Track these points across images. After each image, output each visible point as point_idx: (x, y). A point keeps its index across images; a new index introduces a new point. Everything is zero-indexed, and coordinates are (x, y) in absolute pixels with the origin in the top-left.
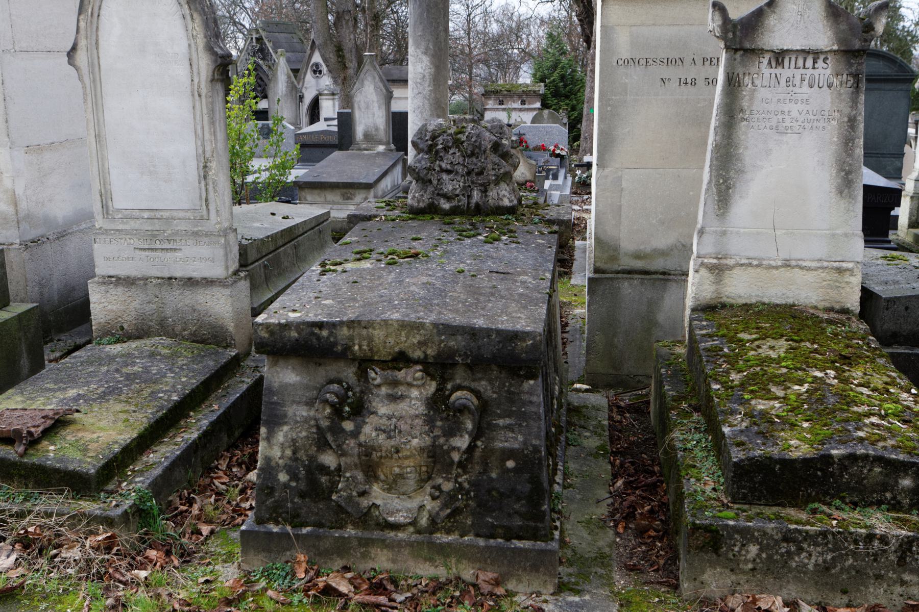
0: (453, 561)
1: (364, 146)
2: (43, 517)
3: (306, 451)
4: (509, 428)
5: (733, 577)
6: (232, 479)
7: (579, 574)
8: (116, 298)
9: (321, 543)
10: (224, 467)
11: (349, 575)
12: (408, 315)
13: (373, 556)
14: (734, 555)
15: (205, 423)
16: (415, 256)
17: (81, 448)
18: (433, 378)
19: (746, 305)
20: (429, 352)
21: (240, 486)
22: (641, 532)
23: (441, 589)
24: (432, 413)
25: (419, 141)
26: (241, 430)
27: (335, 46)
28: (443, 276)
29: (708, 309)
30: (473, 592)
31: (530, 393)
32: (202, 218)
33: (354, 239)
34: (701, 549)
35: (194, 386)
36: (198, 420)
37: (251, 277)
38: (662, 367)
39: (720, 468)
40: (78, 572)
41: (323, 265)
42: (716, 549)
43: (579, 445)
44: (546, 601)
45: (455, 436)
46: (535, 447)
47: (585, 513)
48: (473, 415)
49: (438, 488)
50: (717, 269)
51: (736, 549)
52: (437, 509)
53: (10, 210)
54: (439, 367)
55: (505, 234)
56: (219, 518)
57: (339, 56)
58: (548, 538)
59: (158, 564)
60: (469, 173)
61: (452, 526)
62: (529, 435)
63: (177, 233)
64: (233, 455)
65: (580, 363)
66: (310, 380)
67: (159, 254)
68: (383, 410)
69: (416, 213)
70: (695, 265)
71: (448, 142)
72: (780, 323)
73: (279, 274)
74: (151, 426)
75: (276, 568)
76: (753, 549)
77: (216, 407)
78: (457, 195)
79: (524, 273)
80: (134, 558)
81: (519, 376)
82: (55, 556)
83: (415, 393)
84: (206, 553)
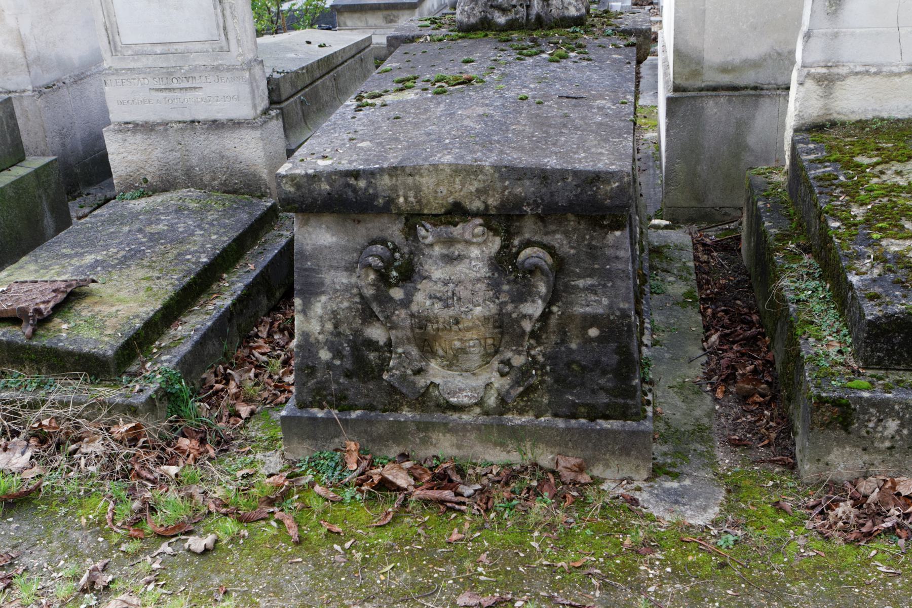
0: (528, 445)
2: (57, 408)
3: (350, 324)
4: (591, 289)
5: (866, 457)
6: (273, 349)
7: (676, 453)
8: (135, 147)
9: (374, 429)
10: (264, 335)
11: (408, 465)
12: (462, 157)
13: (434, 441)
14: (868, 432)
15: (240, 286)
16: (468, 81)
17: (97, 325)
18: (496, 233)
19: (860, 121)
20: (490, 201)
21: (283, 357)
22: (744, 398)
23: (515, 477)
24: (496, 275)
26: (282, 290)
28: (503, 105)
29: (814, 129)
30: (552, 480)
31: (616, 247)
32: (221, 50)
33: (395, 65)
34: (826, 425)
35: (225, 245)
36: (232, 283)
37: (284, 116)
38: (759, 200)
39: (845, 325)
40: (101, 470)
41: (359, 98)
42: (846, 425)
43: (663, 292)
44: (639, 489)
45: (526, 301)
46: (623, 311)
47: (678, 379)
48: (547, 276)
49: (507, 362)
50: (826, 79)
51: (871, 425)
52: (507, 387)
53: (18, 52)
54: (503, 219)
55: (573, 50)
56: (260, 395)
58: (640, 416)
59: (191, 455)
61: (526, 406)
62: (615, 297)
63: (195, 69)
64: (275, 320)
65: (655, 194)
66: (348, 240)
67: (177, 94)
68: (438, 272)
69: (467, 30)
70: (799, 76)
72: (904, 142)
73: (319, 110)
74: (177, 294)
75: (324, 458)
76: (892, 425)
77: (252, 267)
78: (514, 6)
79: (601, 97)
80: (163, 450)
81: (603, 227)
82: (75, 451)
83: (475, 252)
84: (246, 439)
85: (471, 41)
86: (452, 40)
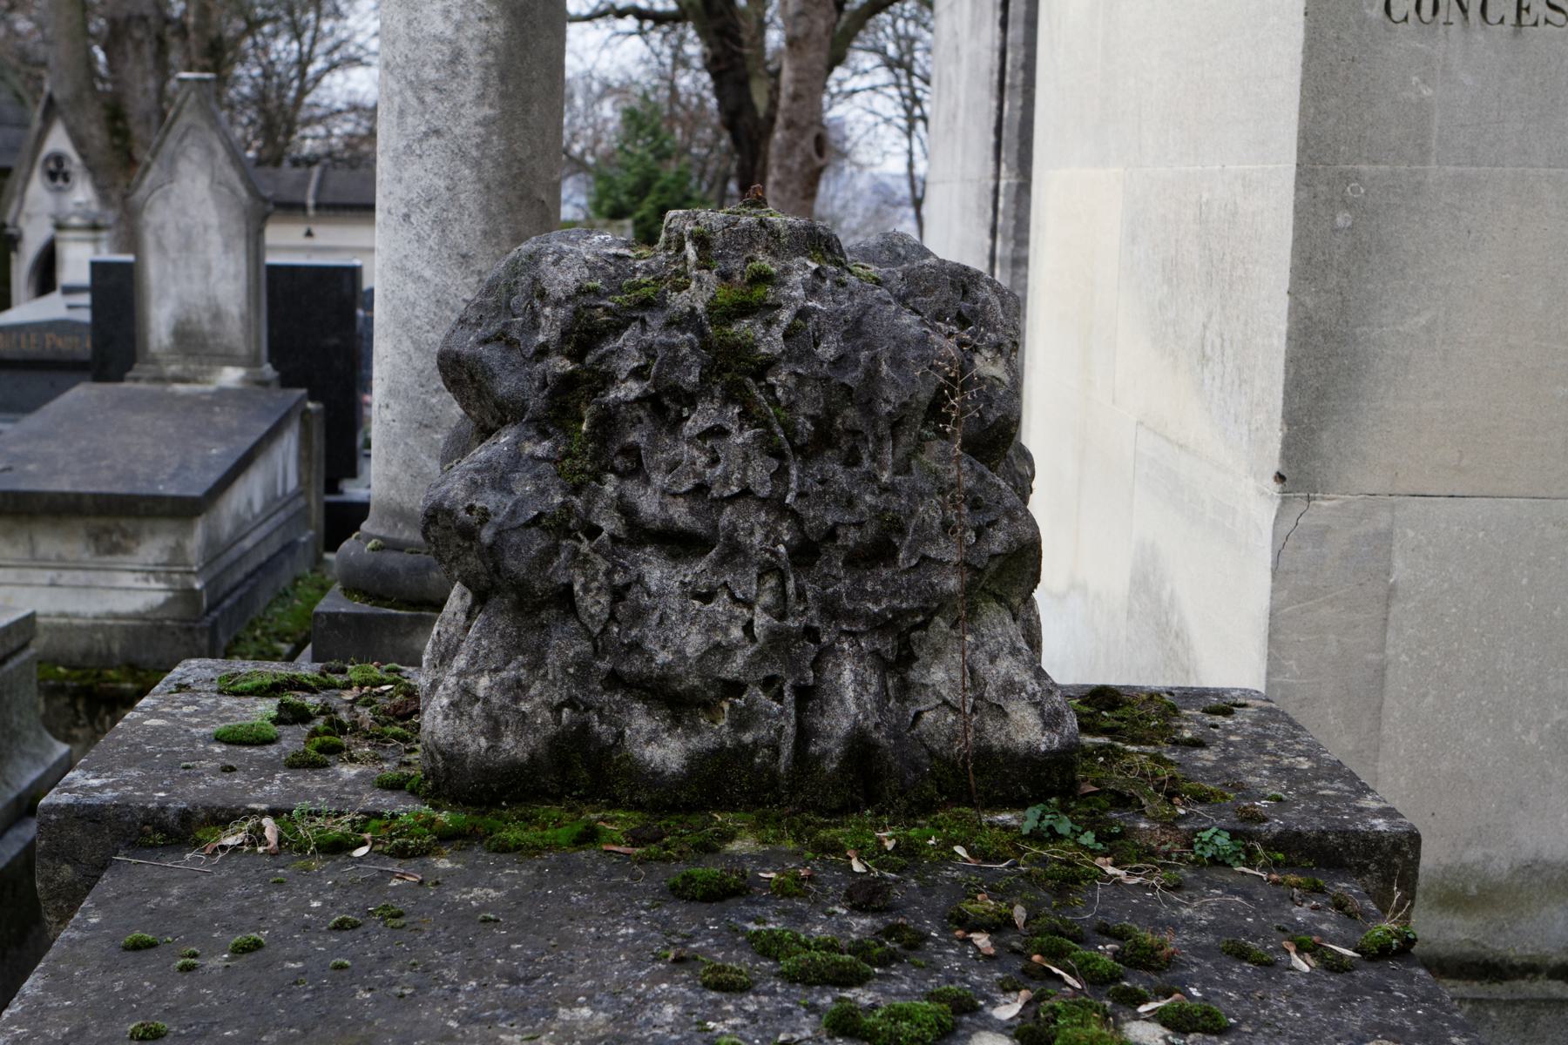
1: (174, 369)
25: (492, 354)
27: (105, 106)
57: (114, 132)
60: (806, 553)
69: (480, 799)
71: (675, 362)
78: (735, 688)
85: (513, 874)
86: (401, 853)
